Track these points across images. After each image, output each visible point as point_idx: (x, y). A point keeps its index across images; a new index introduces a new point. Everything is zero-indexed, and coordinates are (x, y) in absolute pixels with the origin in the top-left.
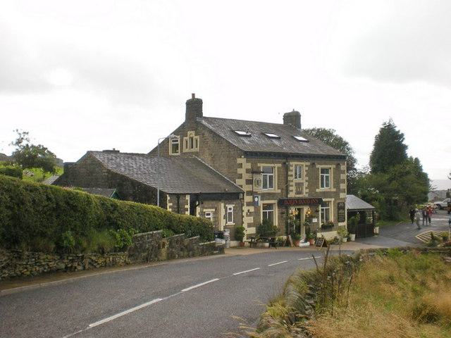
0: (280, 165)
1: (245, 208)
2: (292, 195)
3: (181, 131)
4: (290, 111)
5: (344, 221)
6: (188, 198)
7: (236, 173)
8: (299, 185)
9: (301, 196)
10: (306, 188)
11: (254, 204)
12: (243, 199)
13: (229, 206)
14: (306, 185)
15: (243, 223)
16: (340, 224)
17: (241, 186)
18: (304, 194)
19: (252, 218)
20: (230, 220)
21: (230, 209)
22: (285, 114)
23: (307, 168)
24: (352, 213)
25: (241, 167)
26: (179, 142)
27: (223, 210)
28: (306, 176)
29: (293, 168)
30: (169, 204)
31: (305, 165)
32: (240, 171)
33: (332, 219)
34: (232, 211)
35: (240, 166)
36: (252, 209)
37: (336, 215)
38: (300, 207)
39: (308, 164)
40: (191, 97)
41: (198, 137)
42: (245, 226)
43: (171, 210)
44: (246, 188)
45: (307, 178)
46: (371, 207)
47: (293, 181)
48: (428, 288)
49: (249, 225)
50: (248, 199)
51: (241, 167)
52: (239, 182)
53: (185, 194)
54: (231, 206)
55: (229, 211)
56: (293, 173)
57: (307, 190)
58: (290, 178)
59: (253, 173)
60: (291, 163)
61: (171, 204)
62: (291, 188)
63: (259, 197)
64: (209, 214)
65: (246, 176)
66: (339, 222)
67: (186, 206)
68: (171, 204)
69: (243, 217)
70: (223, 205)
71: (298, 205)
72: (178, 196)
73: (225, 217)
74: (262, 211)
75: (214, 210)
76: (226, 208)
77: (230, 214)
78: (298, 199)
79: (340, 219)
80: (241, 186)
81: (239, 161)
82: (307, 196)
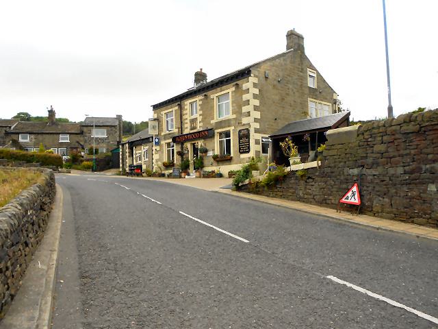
2: (186, 131)
6: (127, 145)
14: (200, 119)
47: (188, 117)
58: (184, 117)
71: (191, 140)
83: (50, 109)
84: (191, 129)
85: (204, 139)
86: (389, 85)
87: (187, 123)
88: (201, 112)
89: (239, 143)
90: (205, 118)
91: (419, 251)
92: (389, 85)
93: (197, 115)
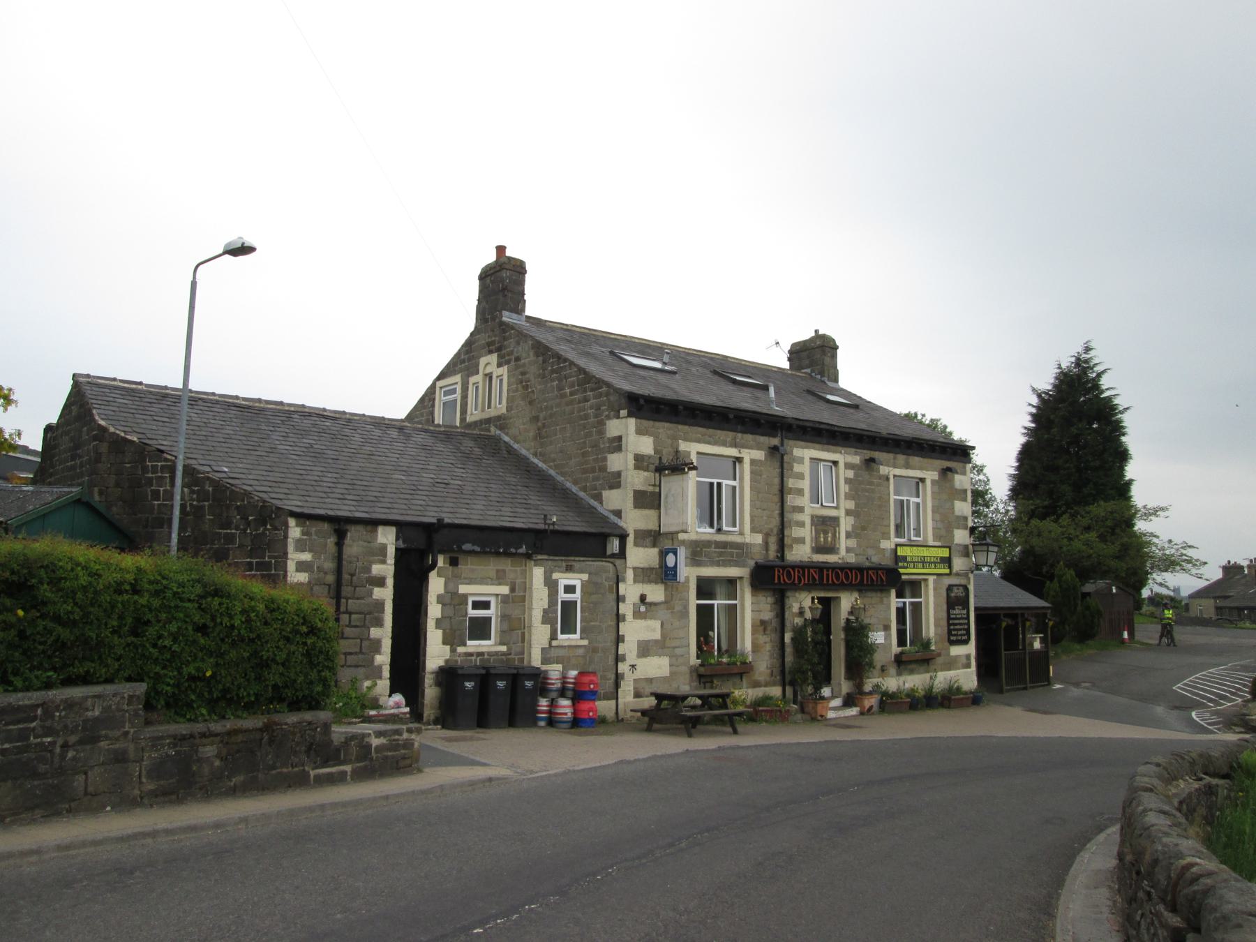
0: (759, 455)
1: (631, 590)
2: (801, 553)
3: (464, 362)
4: (807, 335)
5: (966, 642)
6: (387, 537)
7: (603, 469)
8: (825, 524)
9: (831, 558)
10: (848, 535)
11: (666, 575)
12: (622, 554)
13: (564, 579)
14: (846, 524)
15: (619, 639)
16: (956, 651)
17: (618, 513)
18: (843, 552)
19: (656, 624)
20: (568, 627)
21: (570, 589)
22: (794, 345)
23: (850, 474)
24: (987, 618)
25: (619, 449)
26: (458, 396)
27: (539, 597)
28: (847, 497)
29: (805, 468)
30: (295, 556)
31: (846, 458)
32: (615, 462)
33: (932, 627)
34: (577, 596)
35: (617, 444)
36: (656, 593)
37: (944, 623)
38: (1080, 595)
39: (856, 459)
40: (491, 257)
41: (504, 371)
42: (629, 648)
43: (303, 577)
44: (635, 520)
45: (851, 505)
46: (1034, 601)
47: (805, 508)
48: (801, 608)
49: (645, 649)
50: (638, 556)
51: (619, 449)
52: (614, 499)
53: (374, 523)
54: (576, 580)
55: (563, 596)
56: (805, 485)
57: (852, 543)
58: (791, 500)
59: (660, 469)
60: (797, 452)
61: (306, 556)
62: (796, 532)
63: (682, 552)
64: (486, 605)
65: (637, 480)
66: (952, 643)
67: (376, 569)
68: (306, 556)
69: (619, 618)
70: (538, 573)
71: (822, 586)
72: (340, 526)
73: (548, 618)
74: (693, 602)
75: (505, 590)
76: (552, 585)
77: (569, 607)
78: (821, 568)
79: (955, 636)
80: (618, 513)
81: (614, 427)
82: (851, 559)
83: (860, 407)
84: (819, 549)
85: (860, 591)
86: (194, 284)
87: (802, 524)
88: (851, 505)
89: (949, 618)
90: (864, 528)
91: (191, 656)
92: (194, 284)
93: (840, 508)
